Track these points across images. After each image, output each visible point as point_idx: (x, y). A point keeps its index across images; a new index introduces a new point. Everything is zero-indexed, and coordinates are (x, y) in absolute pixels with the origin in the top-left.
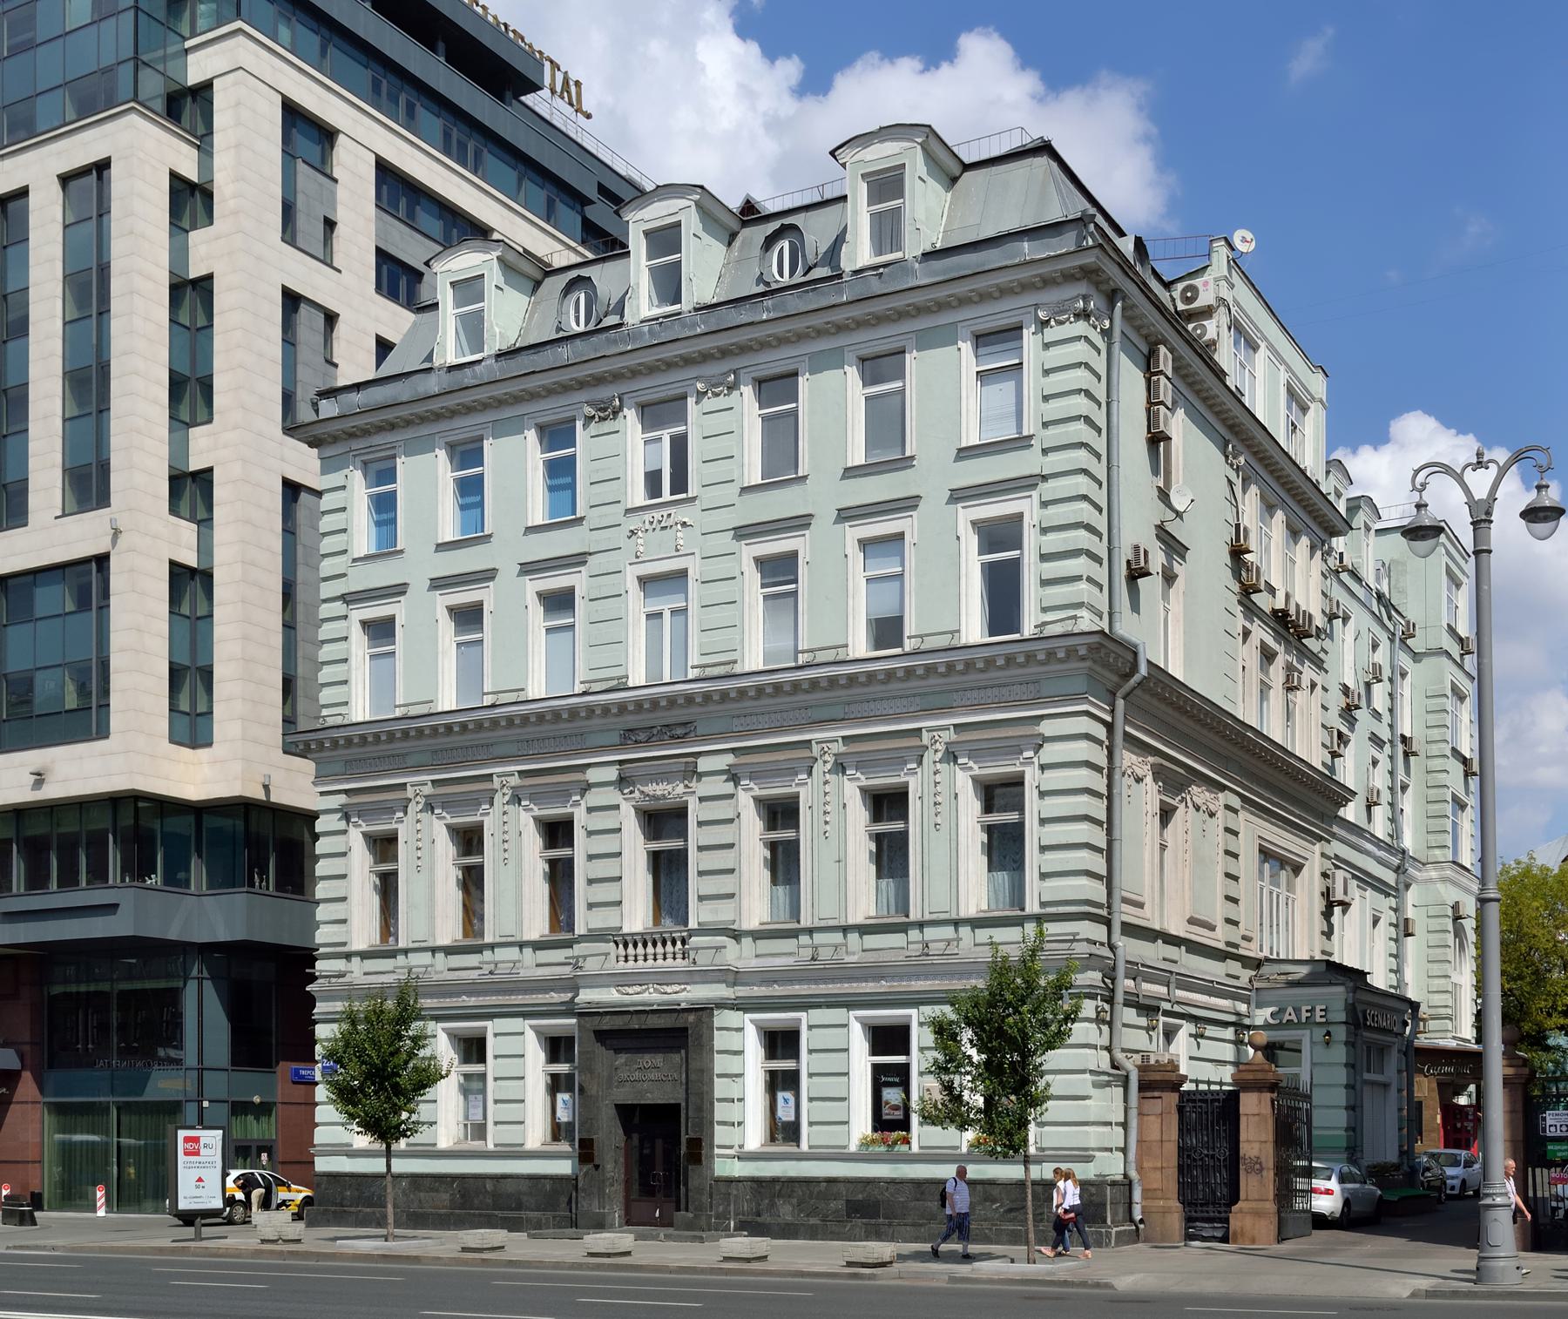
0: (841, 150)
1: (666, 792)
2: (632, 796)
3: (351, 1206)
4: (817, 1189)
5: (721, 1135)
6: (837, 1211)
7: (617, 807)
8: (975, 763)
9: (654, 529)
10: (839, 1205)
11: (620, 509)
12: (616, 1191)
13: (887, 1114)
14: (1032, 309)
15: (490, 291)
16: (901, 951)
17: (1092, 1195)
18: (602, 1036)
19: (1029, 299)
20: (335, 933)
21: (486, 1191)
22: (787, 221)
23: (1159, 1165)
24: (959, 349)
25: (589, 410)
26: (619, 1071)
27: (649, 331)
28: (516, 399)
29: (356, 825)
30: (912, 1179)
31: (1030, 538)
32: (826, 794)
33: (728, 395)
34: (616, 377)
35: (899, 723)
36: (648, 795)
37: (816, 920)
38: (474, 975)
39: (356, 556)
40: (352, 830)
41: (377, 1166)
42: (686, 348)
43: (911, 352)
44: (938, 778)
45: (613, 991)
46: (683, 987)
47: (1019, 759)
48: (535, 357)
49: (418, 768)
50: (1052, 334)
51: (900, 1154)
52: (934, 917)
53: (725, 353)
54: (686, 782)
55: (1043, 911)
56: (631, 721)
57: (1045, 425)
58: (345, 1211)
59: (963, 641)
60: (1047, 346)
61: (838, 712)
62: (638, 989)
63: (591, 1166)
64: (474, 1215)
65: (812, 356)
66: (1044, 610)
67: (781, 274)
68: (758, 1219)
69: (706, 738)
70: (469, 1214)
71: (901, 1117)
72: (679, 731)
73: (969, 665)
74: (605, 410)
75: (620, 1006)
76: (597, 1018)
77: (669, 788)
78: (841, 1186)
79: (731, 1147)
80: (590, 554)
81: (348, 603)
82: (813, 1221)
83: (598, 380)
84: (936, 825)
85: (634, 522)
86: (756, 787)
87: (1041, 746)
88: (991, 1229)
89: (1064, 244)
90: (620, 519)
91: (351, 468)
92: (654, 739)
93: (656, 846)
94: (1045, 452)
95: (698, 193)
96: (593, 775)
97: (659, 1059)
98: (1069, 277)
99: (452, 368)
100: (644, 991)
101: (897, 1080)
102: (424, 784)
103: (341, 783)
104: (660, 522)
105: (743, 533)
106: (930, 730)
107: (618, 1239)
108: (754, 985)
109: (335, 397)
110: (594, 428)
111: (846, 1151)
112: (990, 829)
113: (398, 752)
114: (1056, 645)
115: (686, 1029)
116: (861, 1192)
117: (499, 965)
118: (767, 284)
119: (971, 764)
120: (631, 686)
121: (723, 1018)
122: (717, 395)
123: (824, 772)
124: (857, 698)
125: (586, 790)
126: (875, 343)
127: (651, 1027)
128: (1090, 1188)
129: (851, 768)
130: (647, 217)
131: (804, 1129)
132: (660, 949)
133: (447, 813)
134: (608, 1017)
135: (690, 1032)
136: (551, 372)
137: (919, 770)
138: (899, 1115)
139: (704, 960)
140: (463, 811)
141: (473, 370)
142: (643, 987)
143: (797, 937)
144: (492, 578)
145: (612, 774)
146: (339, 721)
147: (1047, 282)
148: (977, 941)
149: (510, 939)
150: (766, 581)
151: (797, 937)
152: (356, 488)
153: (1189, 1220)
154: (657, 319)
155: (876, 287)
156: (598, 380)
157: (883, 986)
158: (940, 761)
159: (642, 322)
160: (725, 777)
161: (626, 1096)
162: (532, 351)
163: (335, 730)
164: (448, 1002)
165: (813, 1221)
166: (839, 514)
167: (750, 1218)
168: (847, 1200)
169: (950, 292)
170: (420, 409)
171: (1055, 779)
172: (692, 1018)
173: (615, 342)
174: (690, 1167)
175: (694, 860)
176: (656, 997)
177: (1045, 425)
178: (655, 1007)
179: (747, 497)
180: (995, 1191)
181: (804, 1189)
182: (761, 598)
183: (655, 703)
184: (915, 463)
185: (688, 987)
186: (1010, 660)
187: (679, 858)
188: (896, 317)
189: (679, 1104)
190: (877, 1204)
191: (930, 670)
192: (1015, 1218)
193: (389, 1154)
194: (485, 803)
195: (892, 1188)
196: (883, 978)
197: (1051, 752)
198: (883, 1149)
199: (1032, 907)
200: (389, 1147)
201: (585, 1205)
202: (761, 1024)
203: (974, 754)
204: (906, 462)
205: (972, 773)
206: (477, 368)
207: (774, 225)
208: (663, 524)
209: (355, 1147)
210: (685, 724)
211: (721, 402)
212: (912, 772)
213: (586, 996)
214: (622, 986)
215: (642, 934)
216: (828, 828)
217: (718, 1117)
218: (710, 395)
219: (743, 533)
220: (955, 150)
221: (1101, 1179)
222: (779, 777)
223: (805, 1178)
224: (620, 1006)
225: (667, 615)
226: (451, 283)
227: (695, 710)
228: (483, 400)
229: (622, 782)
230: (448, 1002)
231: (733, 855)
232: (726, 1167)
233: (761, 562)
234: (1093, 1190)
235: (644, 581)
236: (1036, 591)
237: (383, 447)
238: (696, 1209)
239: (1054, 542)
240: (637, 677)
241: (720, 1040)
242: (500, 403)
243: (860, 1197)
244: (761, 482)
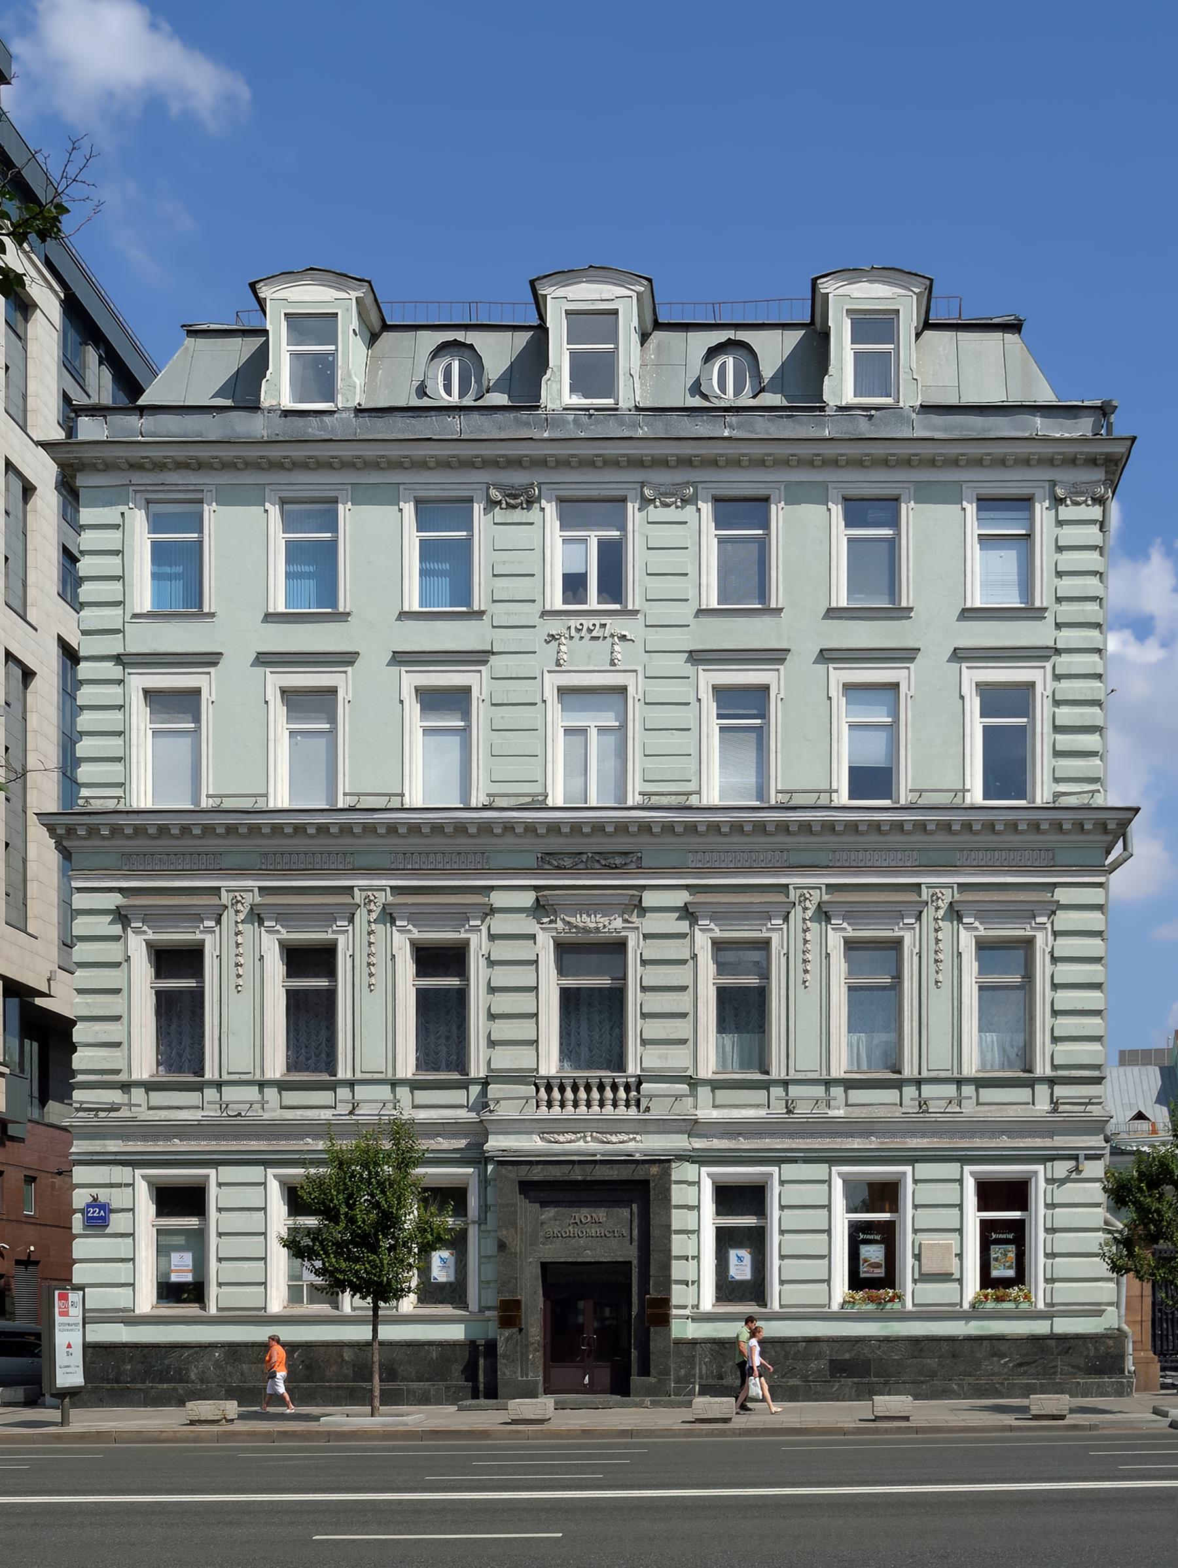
0: (825, 280)
1: (601, 925)
2: (553, 925)
3: (132, 1382)
4: (794, 1350)
5: (678, 1295)
6: (819, 1371)
7: (533, 937)
8: (981, 923)
9: (582, 638)
10: (823, 1364)
11: (537, 608)
12: (536, 1357)
13: (865, 1272)
14: (638, 486)
15: (346, 334)
16: (894, 1107)
17: (1109, 1348)
18: (527, 1187)
19: (638, 475)
20: (104, 1058)
21: (343, 1360)
22: (742, 336)
23: (1139, 1318)
24: (401, 510)
25: (495, 494)
26: (545, 1226)
27: (574, 420)
28: (397, 465)
29: (137, 931)
30: (908, 1337)
31: (1043, 709)
32: (370, 944)
33: (682, 508)
34: (541, 463)
35: (897, 877)
36: (576, 927)
37: (792, 1071)
38: (326, 1114)
39: (137, 611)
40: (132, 937)
41: (363, 1333)
42: (346, 450)
43: (210, 504)
44: (240, 939)
45: (536, 1138)
46: (631, 1136)
47: (1030, 923)
48: (413, 421)
49: (242, 871)
50: (1066, 512)
51: (892, 1311)
52: (933, 1074)
53: (686, 462)
54: (626, 916)
55: (1054, 1074)
56: (556, 843)
57: (1059, 600)
58: (128, 1388)
59: (271, 806)
60: (1060, 523)
61: (822, 858)
62: (573, 1137)
63: (515, 1330)
64: (330, 1388)
65: (788, 485)
66: (1057, 780)
67: (723, 388)
68: (724, 1382)
69: (656, 871)
70: (322, 1387)
71: (883, 1275)
72: (618, 861)
73: (968, 826)
74: (515, 497)
75: (612, 1155)
76: (525, 1168)
77: (605, 920)
78: (824, 1346)
79: (685, 1307)
80: (493, 653)
81: (124, 665)
82: (793, 1382)
83: (516, 463)
84: (370, 985)
85: (555, 626)
86: (717, 929)
87: (1054, 913)
88: (1002, 1384)
89: (1083, 427)
90: (536, 620)
91: (131, 505)
92: (577, 867)
93: (571, 982)
94: (1058, 626)
95: (643, 285)
96: (498, 899)
97: (601, 1214)
98: (1093, 461)
99: (287, 413)
100: (578, 1140)
101: (878, 1237)
102: (382, 889)
103: (118, 879)
104: (590, 631)
105: (697, 657)
106: (930, 886)
107: (544, 1405)
108: (713, 1136)
109: (105, 417)
110: (499, 514)
111: (132, 1314)
112: (159, 994)
113: (209, 849)
114: (1087, 817)
115: (647, 1182)
116: (849, 1351)
117: (230, 1106)
118: (705, 397)
119: (977, 924)
120: (551, 805)
121: (683, 1171)
122: (668, 505)
123: (237, 922)
124: (846, 846)
125: (487, 915)
126: (865, 485)
127: (601, 1178)
128: (1108, 1340)
129: (270, 919)
130: (571, 296)
131: (213, 1291)
132: (582, 1094)
133: (414, 926)
134: (540, 1167)
135: (652, 1185)
136: (395, 443)
137: (350, 928)
138: (880, 1273)
139: (658, 1111)
140: (870, 924)
141: (322, 421)
142: (579, 1135)
143: (201, 1090)
144: (351, 663)
145: (528, 899)
146: (111, 805)
147: (1072, 462)
148: (151, 1104)
149: (376, 1076)
150: (723, 712)
151: (201, 1090)
152: (137, 529)
153: (1163, 1369)
154: (588, 410)
155: (864, 428)
156: (516, 463)
157: (873, 1143)
158: (375, 921)
159: (565, 409)
160: (677, 915)
161: (555, 1252)
162: (410, 414)
163: (124, 816)
164: (283, 1145)
165: (793, 1382)
166: (393, 655)
167: (711, 1382)
168: (832, 1361)
169: (215, 454)
170: (227, 453)
171: (1066, 947)
172: (654, 1170)
173: (527, 424)
174: (652, 1329)
175: (634, 998)
176: (593, 1146)
177: (1059, 600)
178: (598, 1157)
179: (705, 620)
180: (1004, 1347)
181: (779, 1349)
182: (717, 729)
183: (576, 828)
184: (912, 614)
185: (638, 1137)
186: (1013, 826)
187: (615, 999)
188: (196, 466)
189: (630, 1263)
190: (868, 1361)
191: (921, 826)
192: (1025, 1373)
193: (375, 1321)
194: (342, 919)
195: (885, 1346)
196: (871, 1134)
197: (1064, 920)
198: (871, 1307)
199: (1042, 1068)
200: (376, 1308)
201: (507, 1373)
202: (153, 1180)
203: (983, 915)
204: (903, 613)
205: (279, 936)
206: (327, 419)
207: (720, 336)
208: (594, 634)
209: (137, 1312)
210: (626, 854)
211: (671, 513)
212: (910, 927)
213: (496, 1143)
214: (547, 1133)
215: (548, 1078)
216: (808, 977)
217: (675, 1275)
218: (504, 506)
219: (697, 657)
220: (381, 305)
221: (1109, 1332)
222: (748, 919)
223: (780, 1338)
224: (539, 1156)
225: (593, 734)
226: (286, 314)
227: (645, 839)
228: (177, 459)
229: (540, 909)
230: (283, 1145)
231: (686, 998)
232: (683, 1329)
233: (720, 692)
234: (1111, 1343)
235: (563, 691)
236: (1049, 761)
237: (180, 488)
238: (660, 1373)
239: (1067, 715)
240: (557, 798)
241: (678, 1194)
242: (374, 465)
243: (847, 1356)
244: (717, 606)
